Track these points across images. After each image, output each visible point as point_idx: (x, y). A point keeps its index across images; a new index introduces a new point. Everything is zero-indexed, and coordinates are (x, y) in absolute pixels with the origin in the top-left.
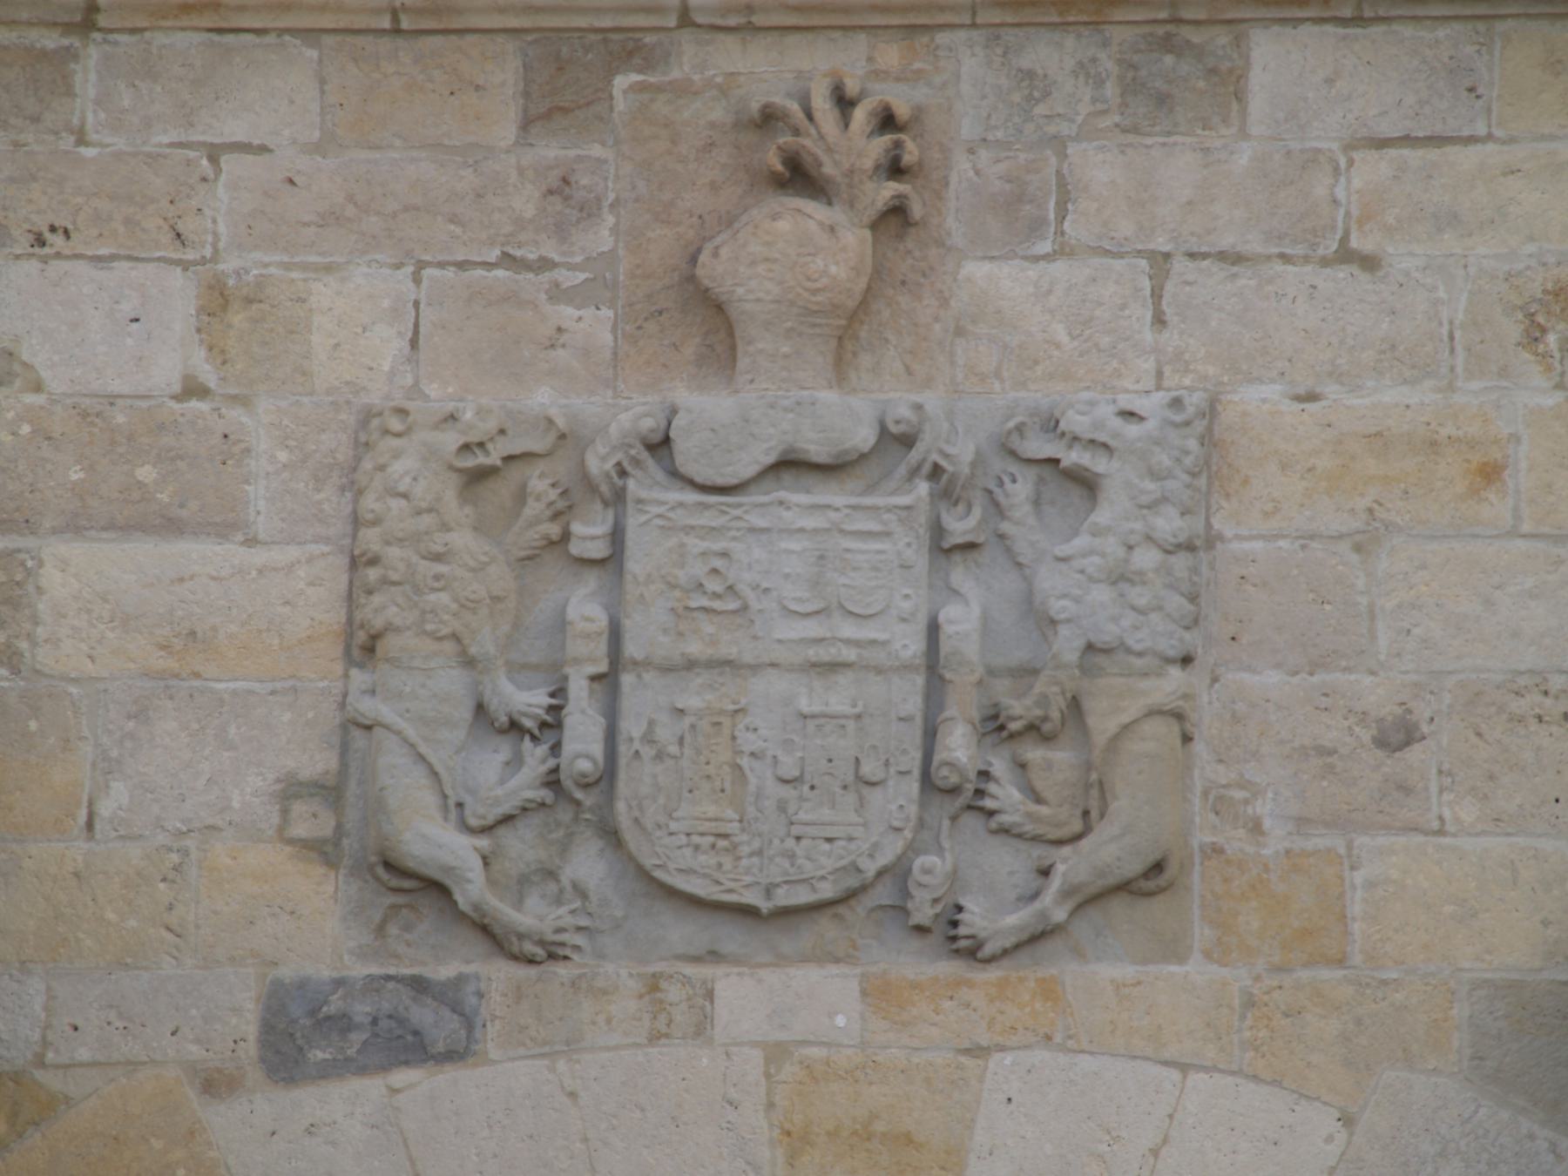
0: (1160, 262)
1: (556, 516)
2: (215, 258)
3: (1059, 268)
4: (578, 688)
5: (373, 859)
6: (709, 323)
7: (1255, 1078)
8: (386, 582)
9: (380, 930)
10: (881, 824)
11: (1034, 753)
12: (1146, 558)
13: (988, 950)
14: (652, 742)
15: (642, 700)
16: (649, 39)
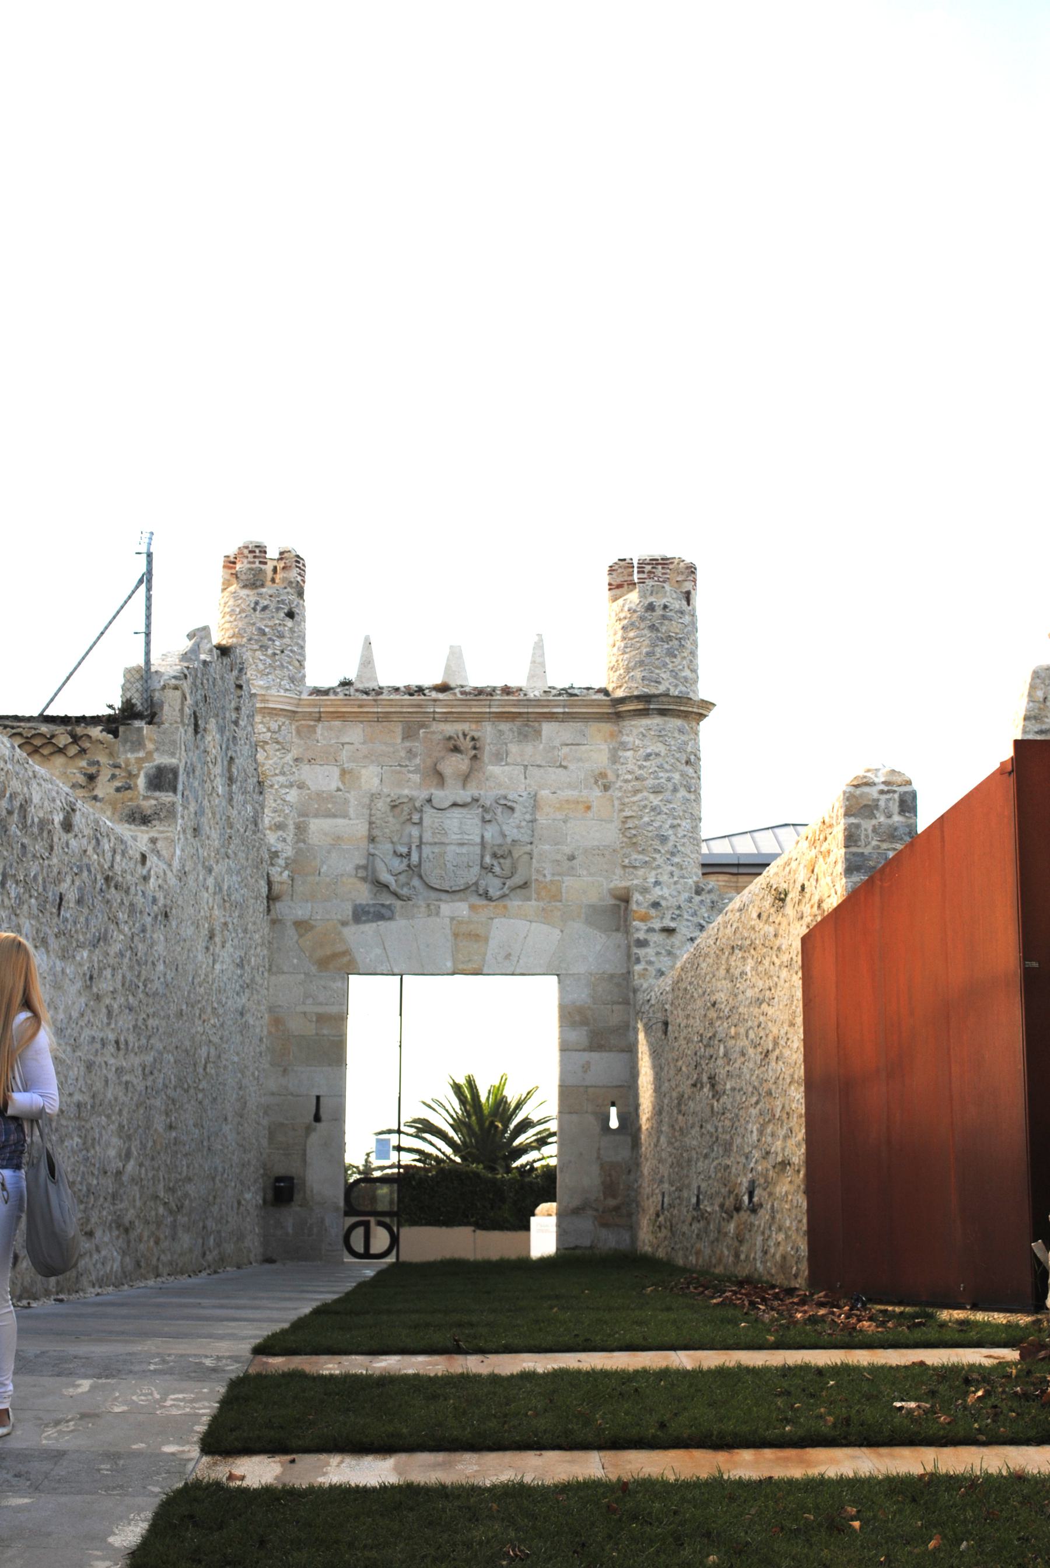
0: (526, 767)
3: (506, 768)
4: (414, 847)
6: (440, 778)
11: (502, 861)
12: (524, 824)
15: (426, 850)
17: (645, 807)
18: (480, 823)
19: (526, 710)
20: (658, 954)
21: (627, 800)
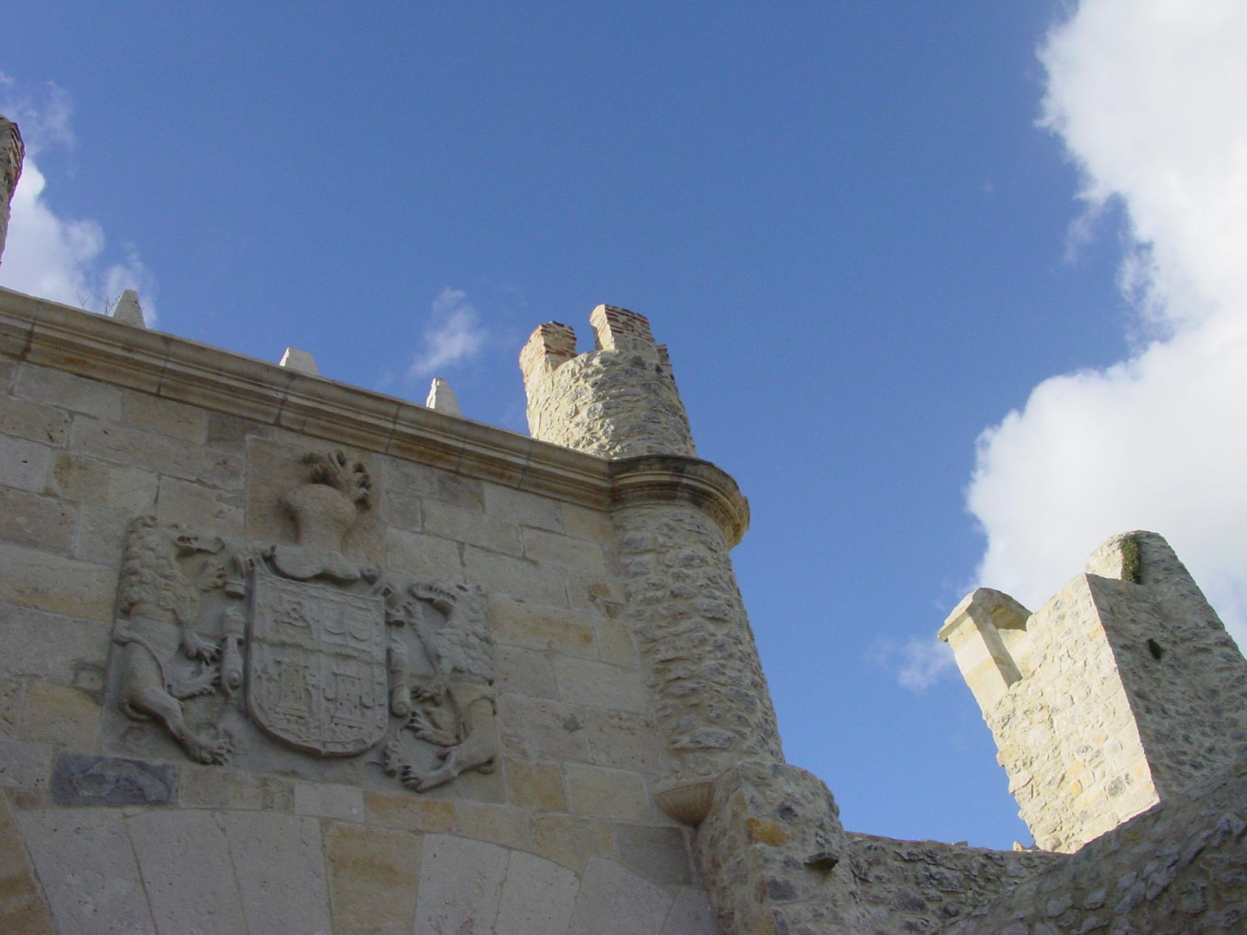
0: (461, 545)
1: (220, 576)
2: (67, 448)
3: (423, 537)
4: (232, 642)
5: (125, 700)
6: (290, 518)
7: (539, 855)
8: (142, 582)
9: (123, 737)
10: (373, 726)
13: (424, 785)
14: (267, 673)
15: (261, 656)
16: (261, 426)
17: (703, 641)
18: (381, 621)
19: (461, 445)
20: (818, 916)
21: (659, 633)
